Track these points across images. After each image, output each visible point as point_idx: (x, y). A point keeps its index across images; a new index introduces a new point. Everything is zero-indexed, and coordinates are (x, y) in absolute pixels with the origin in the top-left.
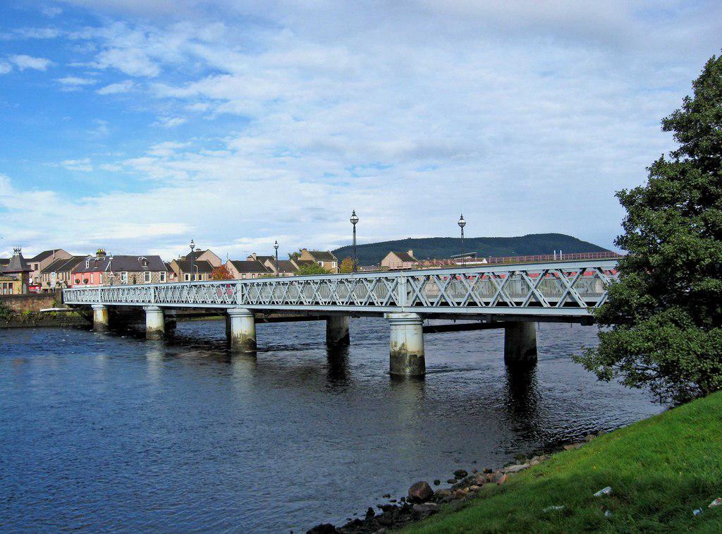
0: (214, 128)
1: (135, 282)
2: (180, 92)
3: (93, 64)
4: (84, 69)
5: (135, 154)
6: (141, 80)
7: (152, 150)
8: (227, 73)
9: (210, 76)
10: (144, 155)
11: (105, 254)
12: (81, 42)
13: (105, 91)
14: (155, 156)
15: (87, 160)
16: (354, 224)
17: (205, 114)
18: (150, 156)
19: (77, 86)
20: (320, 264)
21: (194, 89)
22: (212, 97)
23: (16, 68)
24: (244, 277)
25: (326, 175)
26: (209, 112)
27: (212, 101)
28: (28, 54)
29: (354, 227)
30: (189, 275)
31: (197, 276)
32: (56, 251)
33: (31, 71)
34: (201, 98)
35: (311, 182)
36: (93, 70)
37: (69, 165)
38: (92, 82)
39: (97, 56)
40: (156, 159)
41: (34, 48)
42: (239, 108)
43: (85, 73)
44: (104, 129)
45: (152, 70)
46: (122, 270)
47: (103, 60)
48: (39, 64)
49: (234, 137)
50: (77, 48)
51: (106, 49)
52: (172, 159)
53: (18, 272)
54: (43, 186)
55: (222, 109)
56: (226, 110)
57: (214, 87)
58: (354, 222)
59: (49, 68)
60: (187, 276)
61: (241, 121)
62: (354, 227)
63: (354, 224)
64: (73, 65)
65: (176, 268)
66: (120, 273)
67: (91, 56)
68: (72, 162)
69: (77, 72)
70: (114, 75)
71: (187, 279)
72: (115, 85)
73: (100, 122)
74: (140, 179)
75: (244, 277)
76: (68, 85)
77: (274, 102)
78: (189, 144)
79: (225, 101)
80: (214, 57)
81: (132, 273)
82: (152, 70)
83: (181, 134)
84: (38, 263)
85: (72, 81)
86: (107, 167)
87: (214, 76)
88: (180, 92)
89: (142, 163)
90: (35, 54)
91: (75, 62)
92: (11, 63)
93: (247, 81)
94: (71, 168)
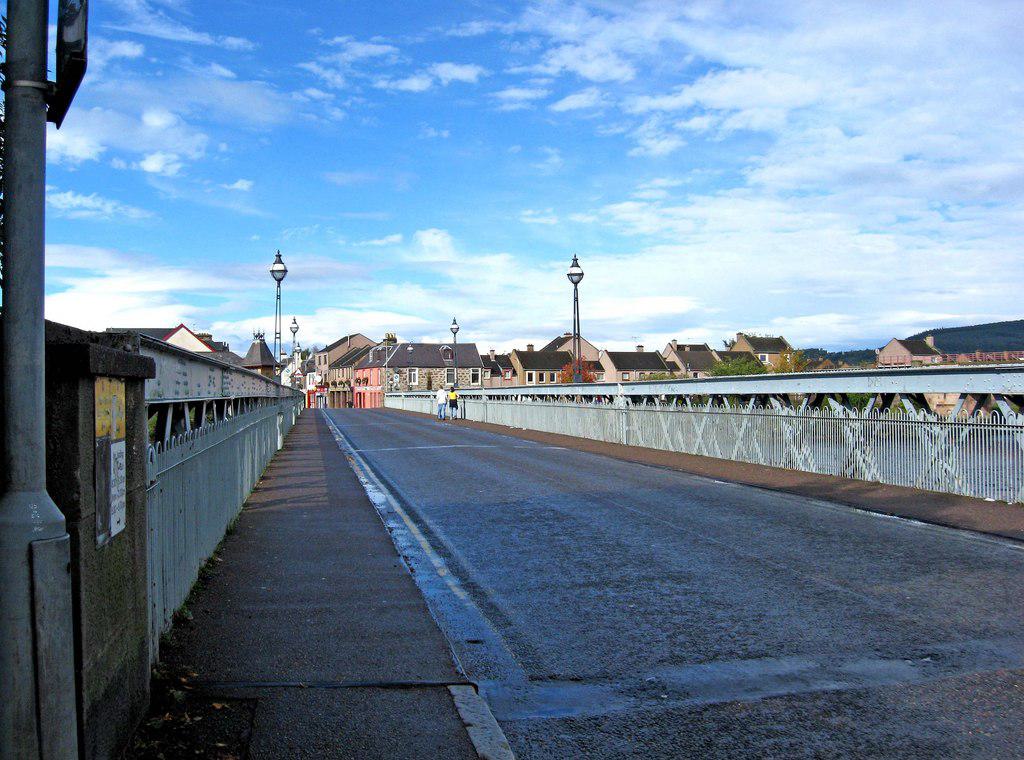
0: (722, 159)
1: (429, 387)
2: (668, 103)
3: (539, 68)
4: (529, 76)
5: (613, 199)
6: (607, 85)
7: (637, 191)
8: (735, 69)
9: (709, 74)
10: (627, 199)
11: (395, 340)
12: (521, 37)
13: (562, 106)
14: (642, 200)
15: (549, 210)
16: (576, 284)
17: (708, 134)
18: (636, 200)
19: (523, 101)
20: (763, 358)
21: (688, 96)
22: (715, 107)
23: (437, 81)
24: (626, 377)
25: (901, 219)
26: (715, 130)
27: (718, 111)
28: (451, 61)
29: (576, 289)
30: (534, 373)
31: (546, 375)
32: (351, 337)
33: (459, 86)
34: (697, 110)
35: (876, 232)
36: (541, 76)
37: (527, 216)
38: (542, 94)
39: (544, 56)
40: (645, 204)
41: (459, 51)
42: (758, 120)
43: (532, 81)
44: (556, 160)
45: (624, 73)
46: (410, 365)
47: (552, 61)
48: (468, 73)
49: (755, 166)
50: (516, 47)
51: (557, 45)
52: (666, 203)
53: (257, 368)
54: (495, 247)
55: (733, 124)
56: (739, 126)
57: (710, 91)
58: (576, 279)
59: (480, 77)
60: (530, 376)
61: (760, 141)
62: (576, 289)
63: (576, 284)
64: (515, 70)
65: (517, 363)
66: (406, 370)
67: (536, 57)
68: (530, 212)
69: (519, 81)
70: (569, 82)
71: (530, 379)
72: (572, 96)
73: (549, 150)
74: (624, 233)
75: (626, 377)
76: (512, 101)
77: (797, 115)
78: (689, 180)
79: (735, 111)
80: (705, 44)
81: (425, 370)
82: (624, 73)
83: (675, 163)
84: (326, 354)
85: (515, 96)
86: (578, 218)
87: (715, 72)
88: (668, 103)
89: (625, 210)
90: (461, 60)
91: (514, 66)
92: (431, 75)
93: (759, 84)
94: (528, 220)
